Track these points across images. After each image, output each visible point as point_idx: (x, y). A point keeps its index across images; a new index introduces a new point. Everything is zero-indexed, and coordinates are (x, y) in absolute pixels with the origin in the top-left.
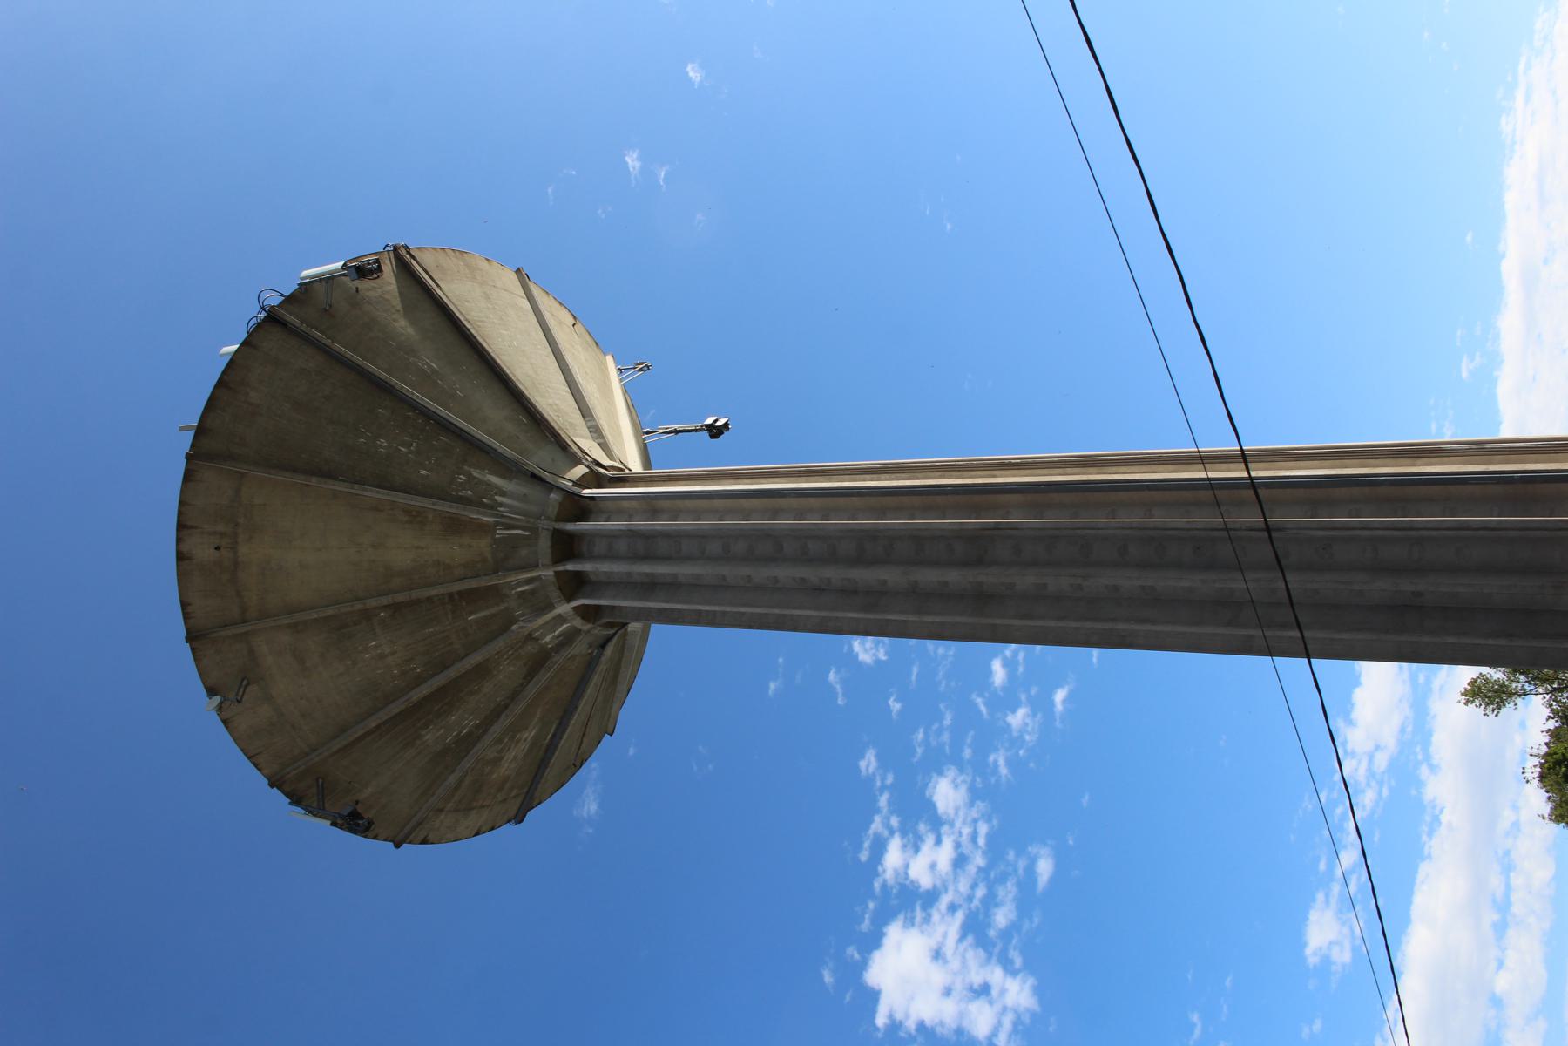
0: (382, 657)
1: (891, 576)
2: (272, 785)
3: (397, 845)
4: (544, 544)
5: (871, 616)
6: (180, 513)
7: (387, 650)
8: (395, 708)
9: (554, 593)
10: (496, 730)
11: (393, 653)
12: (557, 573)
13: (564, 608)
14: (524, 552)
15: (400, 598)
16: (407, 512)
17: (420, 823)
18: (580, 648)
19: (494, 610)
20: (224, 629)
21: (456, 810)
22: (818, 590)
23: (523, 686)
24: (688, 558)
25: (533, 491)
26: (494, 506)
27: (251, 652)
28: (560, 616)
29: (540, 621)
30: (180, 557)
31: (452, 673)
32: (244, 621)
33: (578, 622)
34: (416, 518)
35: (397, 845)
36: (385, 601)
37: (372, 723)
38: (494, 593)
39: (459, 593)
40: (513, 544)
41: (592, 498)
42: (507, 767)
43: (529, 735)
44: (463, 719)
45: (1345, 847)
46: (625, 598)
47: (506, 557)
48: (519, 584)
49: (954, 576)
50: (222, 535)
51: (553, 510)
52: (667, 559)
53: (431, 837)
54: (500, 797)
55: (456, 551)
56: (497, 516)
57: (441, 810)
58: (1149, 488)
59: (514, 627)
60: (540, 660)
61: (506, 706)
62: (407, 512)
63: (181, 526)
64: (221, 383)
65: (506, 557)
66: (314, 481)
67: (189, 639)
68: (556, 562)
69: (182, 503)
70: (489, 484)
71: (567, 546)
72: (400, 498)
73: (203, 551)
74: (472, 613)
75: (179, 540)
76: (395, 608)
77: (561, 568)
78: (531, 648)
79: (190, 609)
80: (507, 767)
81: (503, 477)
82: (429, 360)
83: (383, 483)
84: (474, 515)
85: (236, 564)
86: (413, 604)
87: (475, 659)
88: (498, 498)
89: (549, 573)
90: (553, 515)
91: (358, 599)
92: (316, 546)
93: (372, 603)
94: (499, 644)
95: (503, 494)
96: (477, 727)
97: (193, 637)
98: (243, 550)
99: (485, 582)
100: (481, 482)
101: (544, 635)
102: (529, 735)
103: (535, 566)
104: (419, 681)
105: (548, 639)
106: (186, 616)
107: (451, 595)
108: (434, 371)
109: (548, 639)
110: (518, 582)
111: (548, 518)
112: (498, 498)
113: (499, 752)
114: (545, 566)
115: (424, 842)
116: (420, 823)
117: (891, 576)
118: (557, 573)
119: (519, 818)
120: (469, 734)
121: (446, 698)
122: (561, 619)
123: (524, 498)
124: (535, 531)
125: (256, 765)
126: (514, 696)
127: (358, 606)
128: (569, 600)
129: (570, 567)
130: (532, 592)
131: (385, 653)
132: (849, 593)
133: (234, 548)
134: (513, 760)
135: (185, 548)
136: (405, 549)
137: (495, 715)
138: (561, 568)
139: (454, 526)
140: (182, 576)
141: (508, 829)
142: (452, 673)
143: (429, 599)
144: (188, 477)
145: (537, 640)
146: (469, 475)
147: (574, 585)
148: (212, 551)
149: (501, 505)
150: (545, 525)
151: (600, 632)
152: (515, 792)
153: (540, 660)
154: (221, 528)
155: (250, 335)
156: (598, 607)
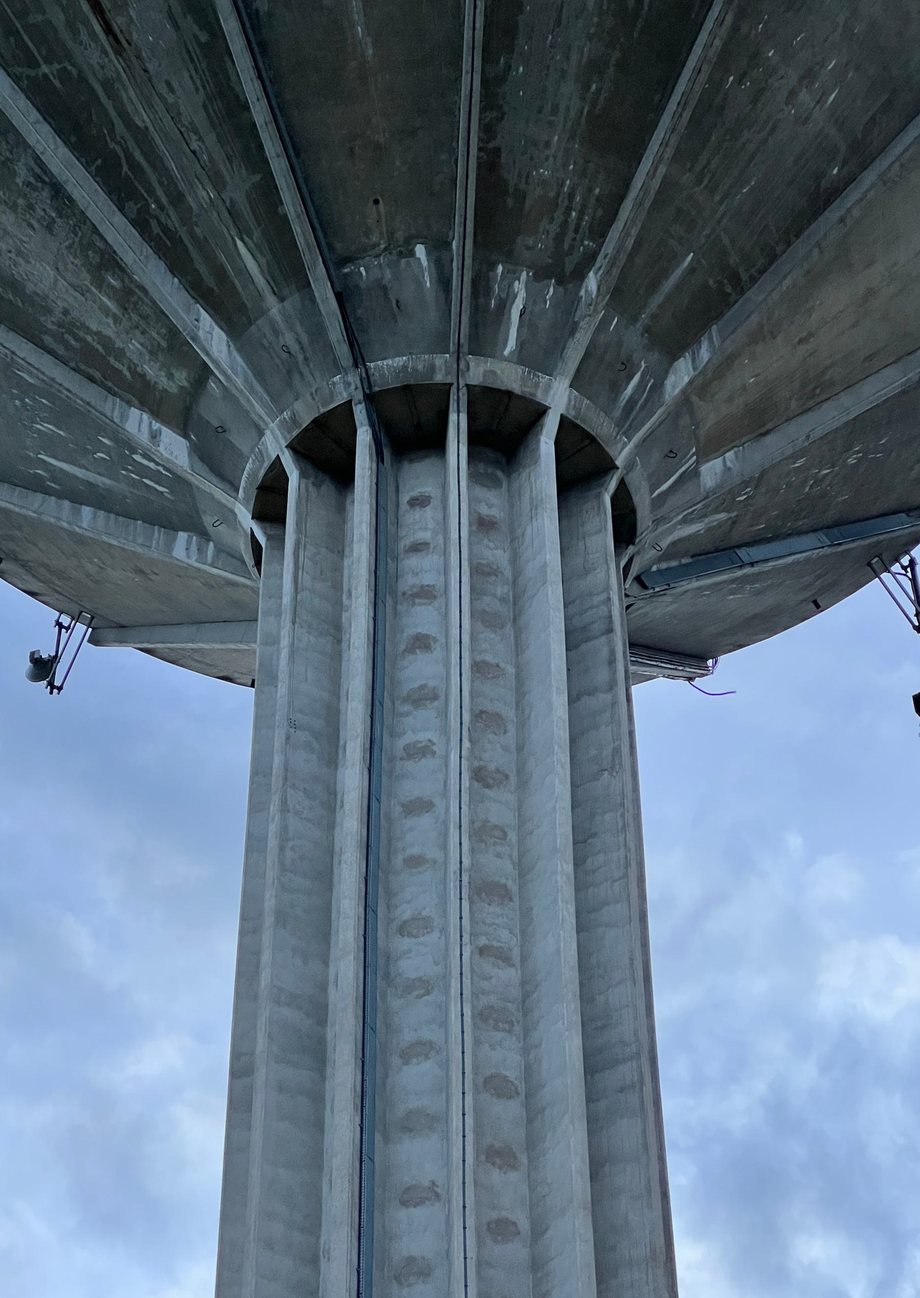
0: (808, 76)
7: (804, 96)
11: (793, 94)
13: (275, 444)
19: (656, 301)
23: (488, 130)
74: (691, 270)
77: (360, 413)
78: (537, 243)
105: (519, 287)
109: (519, 287)
138: (360, 413)
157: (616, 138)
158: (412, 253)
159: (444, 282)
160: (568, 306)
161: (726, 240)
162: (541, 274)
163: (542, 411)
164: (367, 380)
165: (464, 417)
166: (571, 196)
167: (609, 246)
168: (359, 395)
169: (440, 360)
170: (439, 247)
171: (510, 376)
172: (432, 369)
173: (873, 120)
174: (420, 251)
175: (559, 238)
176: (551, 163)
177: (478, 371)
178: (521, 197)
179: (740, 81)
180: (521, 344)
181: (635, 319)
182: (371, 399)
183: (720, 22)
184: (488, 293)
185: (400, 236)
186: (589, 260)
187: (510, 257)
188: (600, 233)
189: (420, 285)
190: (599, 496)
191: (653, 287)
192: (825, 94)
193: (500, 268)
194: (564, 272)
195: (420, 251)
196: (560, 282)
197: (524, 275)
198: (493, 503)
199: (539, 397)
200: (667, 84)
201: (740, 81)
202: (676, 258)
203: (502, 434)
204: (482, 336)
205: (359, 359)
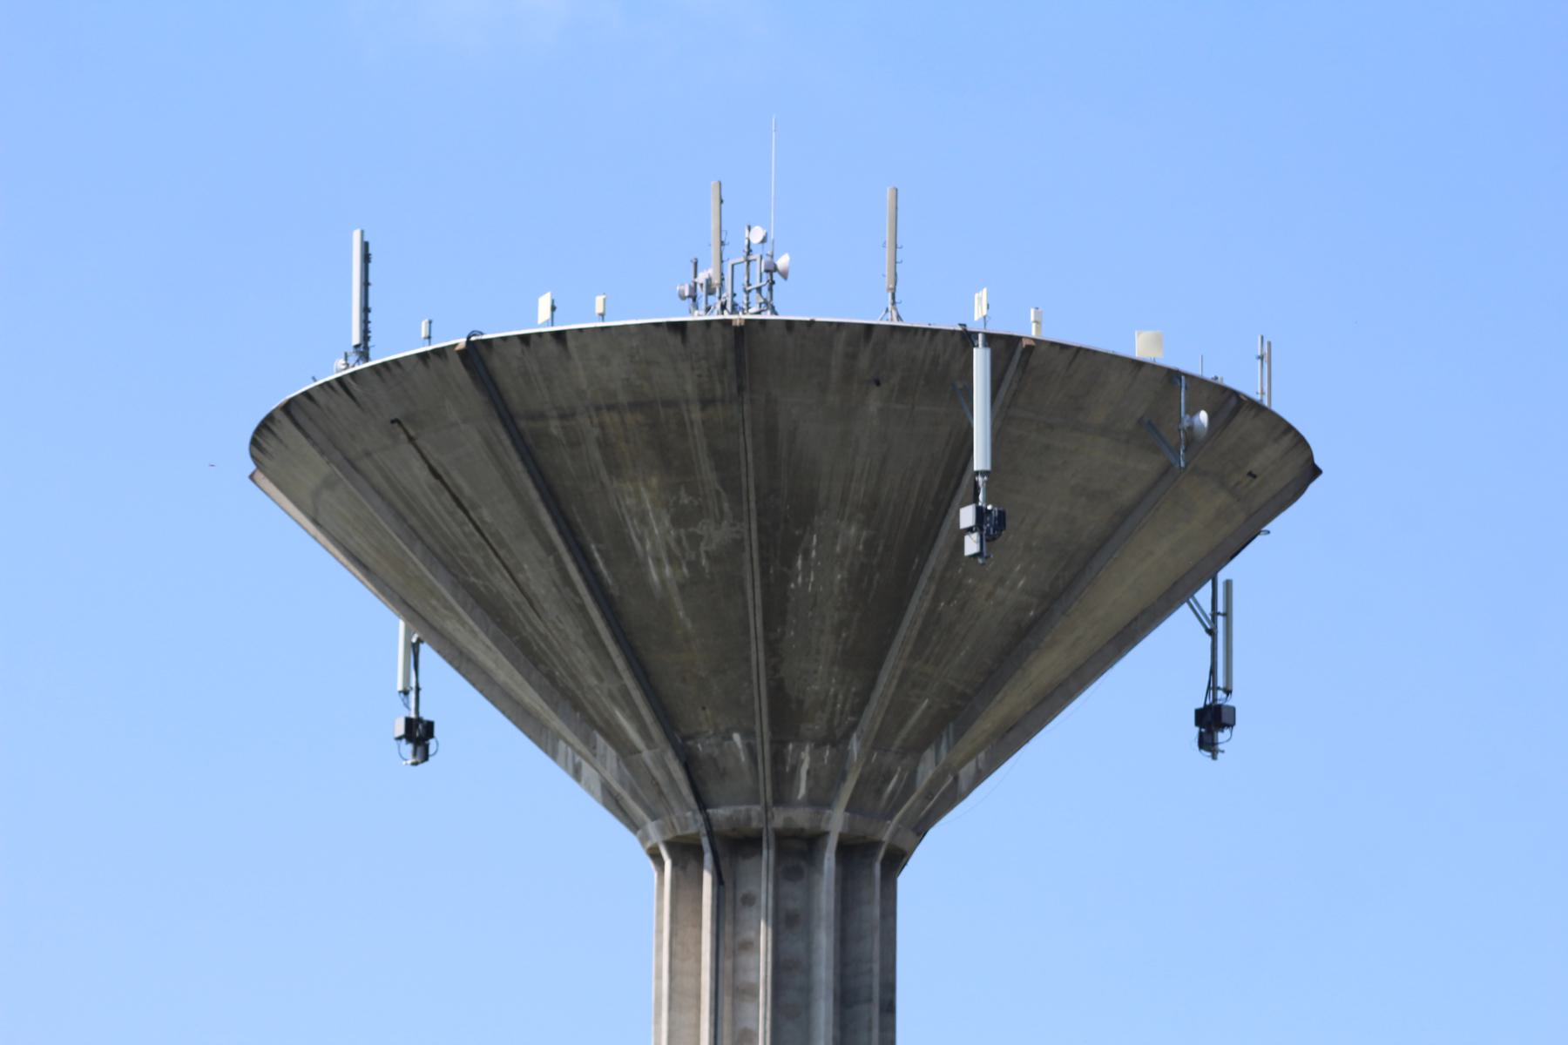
0: (1001, 581)
12: (878, 844)
19: (903, 733)
23: (773, 669)
74: (929, 707)
78: (817, 726)
89: (886, 837)
105: (806, 757)
109: (806, 757)
118: (878, 844)
120: (789, 563)
128: (841, 836)
157: (864, 660)
158: (730, 738)
159: (751, 749)
160: (842, 758)
162: (819, 744)
163: (825, 834)
164: (708, 821)
165: (772, 853)
166: (836, 696)
167: (865, 723)
168: (704, 831)
169: (756, 809)
170: (748, 734)
171: (801, 817)
172: (749, 819)
174: (736, 737)
176: (819, 679)
177: (779, 818)
178: (800, 703)
179: (948, 603)
180: (809, 790)
182: (710, 834)
183: (925, 592)
184: (784, 762)
185: (722, 728)
186: (854, 727)
187: (800, 741)
188: (858, 710)
189: (738, 760)
190: (871, 866)
193: (791, 746)
194: (836, 740)
195: (736, 737)
196: (834, 745)
197: (807, 748)
199: (824, 827)
200: (896, 624)
201: (948, 603)
203: (798, 850)
204: (781, 797)
205: (703, 804)
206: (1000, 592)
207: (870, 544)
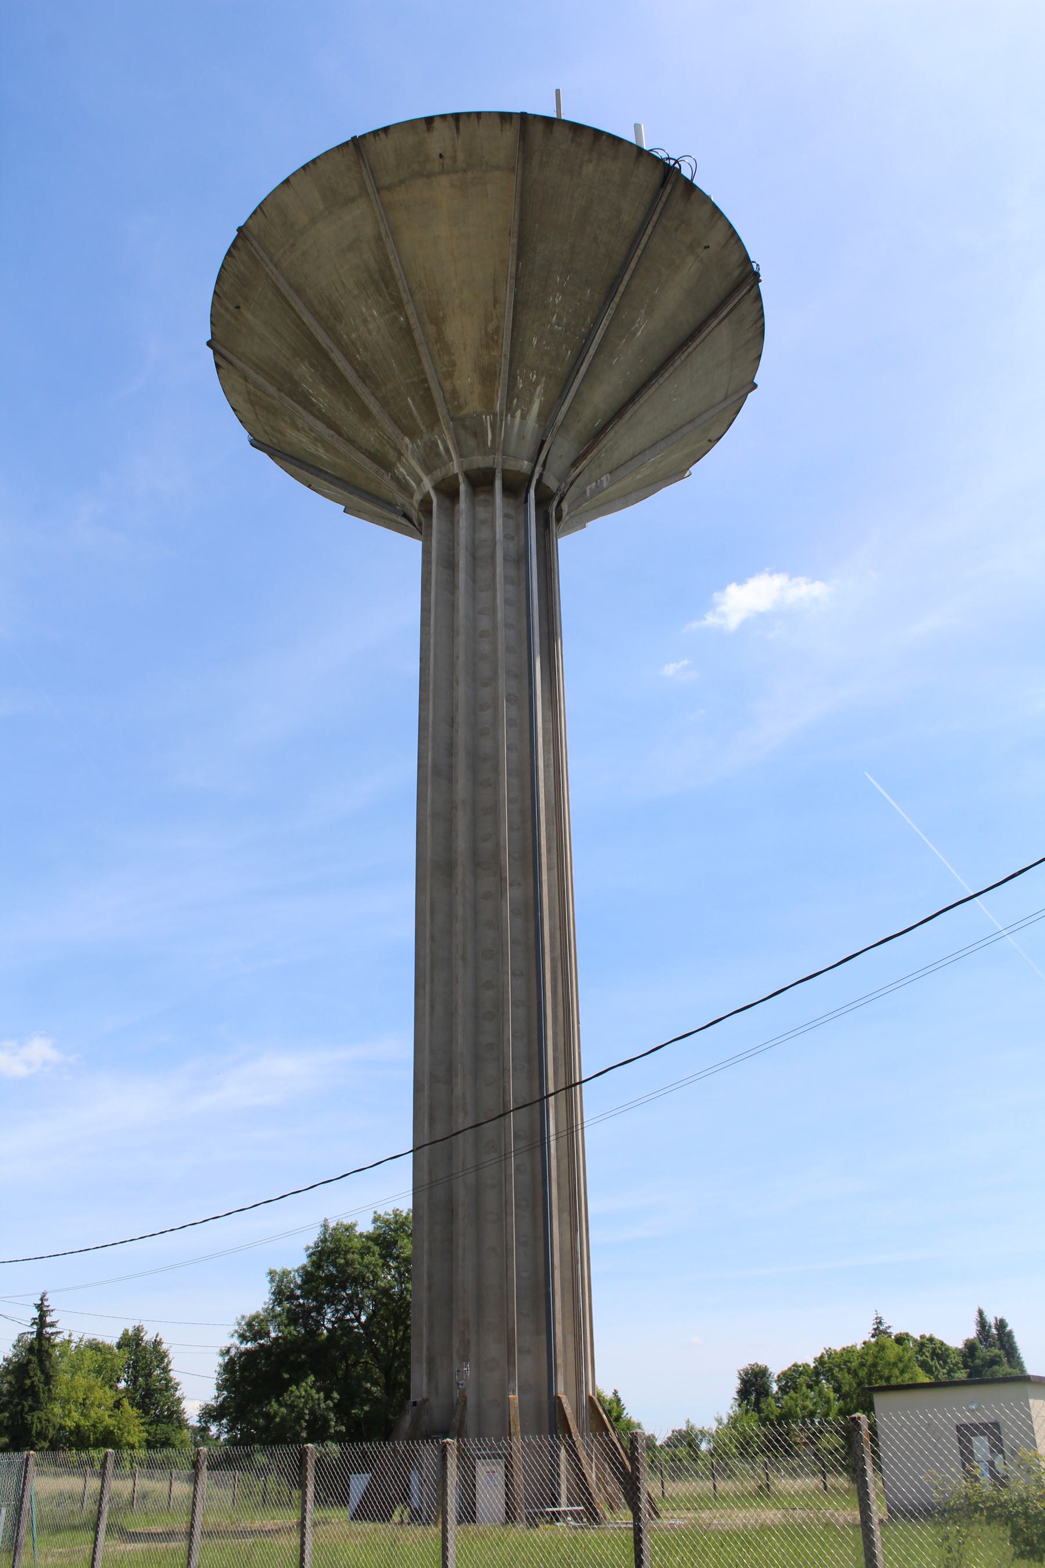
0: (365, 322)
1: (462, 787)
2: (240, 230)
3: (209, 344)
4: (480, 461)
5: (429, 773)
6: (469, 114)
7: (371, 326)
8: (322, 337)
9: (439, 474)
10: (321, 427)
11: (369, 332)
12: (456, 476)
13: (428, 485)
14: (472, 442)
15: (417, 335)
16: (497, 330)
17: (231, 363)
18: (400, 498)
19: (419, 421)
20: (371, 166)
21: (249, 393)
22: (452, 723)
23: (359, 448)
24: (473, 598)
25: (528, 446)
26: (509, 409)
27: (353, 200)
28: (421, 480)
29: (414, 464)
30: (429, 121)
31: (361, 389)
32: (378, 190)
33: (418, 497)
34: (490, 340)
35: (209, 344)
36: (413, 321)
37: (307, 318)
38: (434, 421)
39: (429, 389)
40: (478, 433)
41: (526, 500)
42: (292, 435)
43: (321, 453)
44: (322, 397)
45: (853, 1526)
46: (438, 542)
47: (469, 429)
48: (444, 442)
49: (462, 844)
50: (454, 159)
51: (512, 465)
52: (473, 578)
53: (222, 371)
54: (267, 428)
55: (466, 380)
56: (501, 415)
57: (246, 380)
58: (539, 1004)
59: (407, 440)
60: (385, 465)
61: (340, 435)
62: (497, 330)
63: (457, 117)
64: (598, 134)
65: (469, 429)
66: (514, 241)
67: (354, 139)
68: (467, 475)
69: (479, 114)
70: (531, 402)
71: (480, 481)
72: (507, 324)
73: (438, 141)
74: (413, 400)
75: (443, 117)
76: (408, 330)
77: (461, 479)
78: (392, 455)
79: (382, 135)
80: (292, 435)
81: (540, 414)
82: (644, 328)
83: (518, 305)
84: (501, 392)
85: (429, 176)
86: (413, 346)
87: (374, 407)
88: (519, 412)
89: (455, 467)
90: (506, 467)
91: (412, 294)
92: (457, 244)
93: (410, 309)
94: (390, 428)
95: (523, 417)
96: (320, 410)
97: (356, 143)
98: (444, 180)
99: (442, 411)
100: (532, 395)
101: (404, 466)
102: (321, 453)
103: (461, 455)
104: (347, 355)
105: (402, 469)
106: (375, 133)
107: (425, 380)
108: (635, 333)
109: (402, 469)
110: (445, 440)
111: (504, 462)
112: (519, 412)
113: (303, 429)
114: (461, 465)
115: (217, 366)
116: (231, 363)
117: (462, 787)
118: (456, 476)
119: (257, 443)
120: (313, 404)
121: (337, 382)
122: (419, 482)
123: (522, 436)
124: (493, 450)
125: (254, 213)
126: (351, 442)
127: (405, 297)
128: (436, 488)
129: (463, 488)
130: (438, 454)
131: (369, 323)
132: (451, 749)
133: (443, 172)
134: (298, 439)
135: (437, 124)
136: (463, 331)
137: (332, 426)
138: (461, 479)
139: (487, 376)
140: (412, 124)
141: (244, 435)
142: (361, 389)
143: (419, 361)
144: (505, 117)
145: (399, 459)
146: (537, 383)
147: (448, 491)
148: (439, 151)
149: (513, 417)
150: (496, 461)
151: (414, 514)
152: (275, 441)
153: (385, 465)
154: (461, 157)
155: (648, 154)
156: (430, 512)
161: (408, 381)
173: (390, 294)
175: (391, 447)
176: (369, 437)
178: (378, 450)
181: (422, 431)
191: (414, 420)
192: (372, 316)
198: (482, 513)
199: (425, 491)
202: (408, 405)
206: (371, 326)
207: (312, 365)
